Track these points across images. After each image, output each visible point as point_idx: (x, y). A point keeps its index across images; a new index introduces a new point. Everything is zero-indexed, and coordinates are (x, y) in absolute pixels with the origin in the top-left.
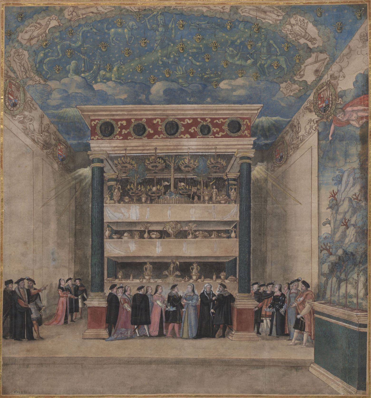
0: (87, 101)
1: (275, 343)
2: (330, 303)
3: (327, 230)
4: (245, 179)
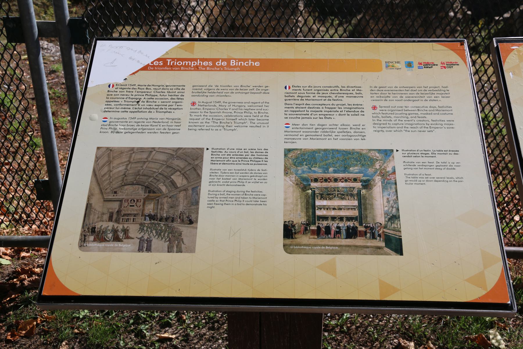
0: (309, 172)
1: (372, 241)
2: (389, 229)
3: (386, 209)
4: (359, 194)
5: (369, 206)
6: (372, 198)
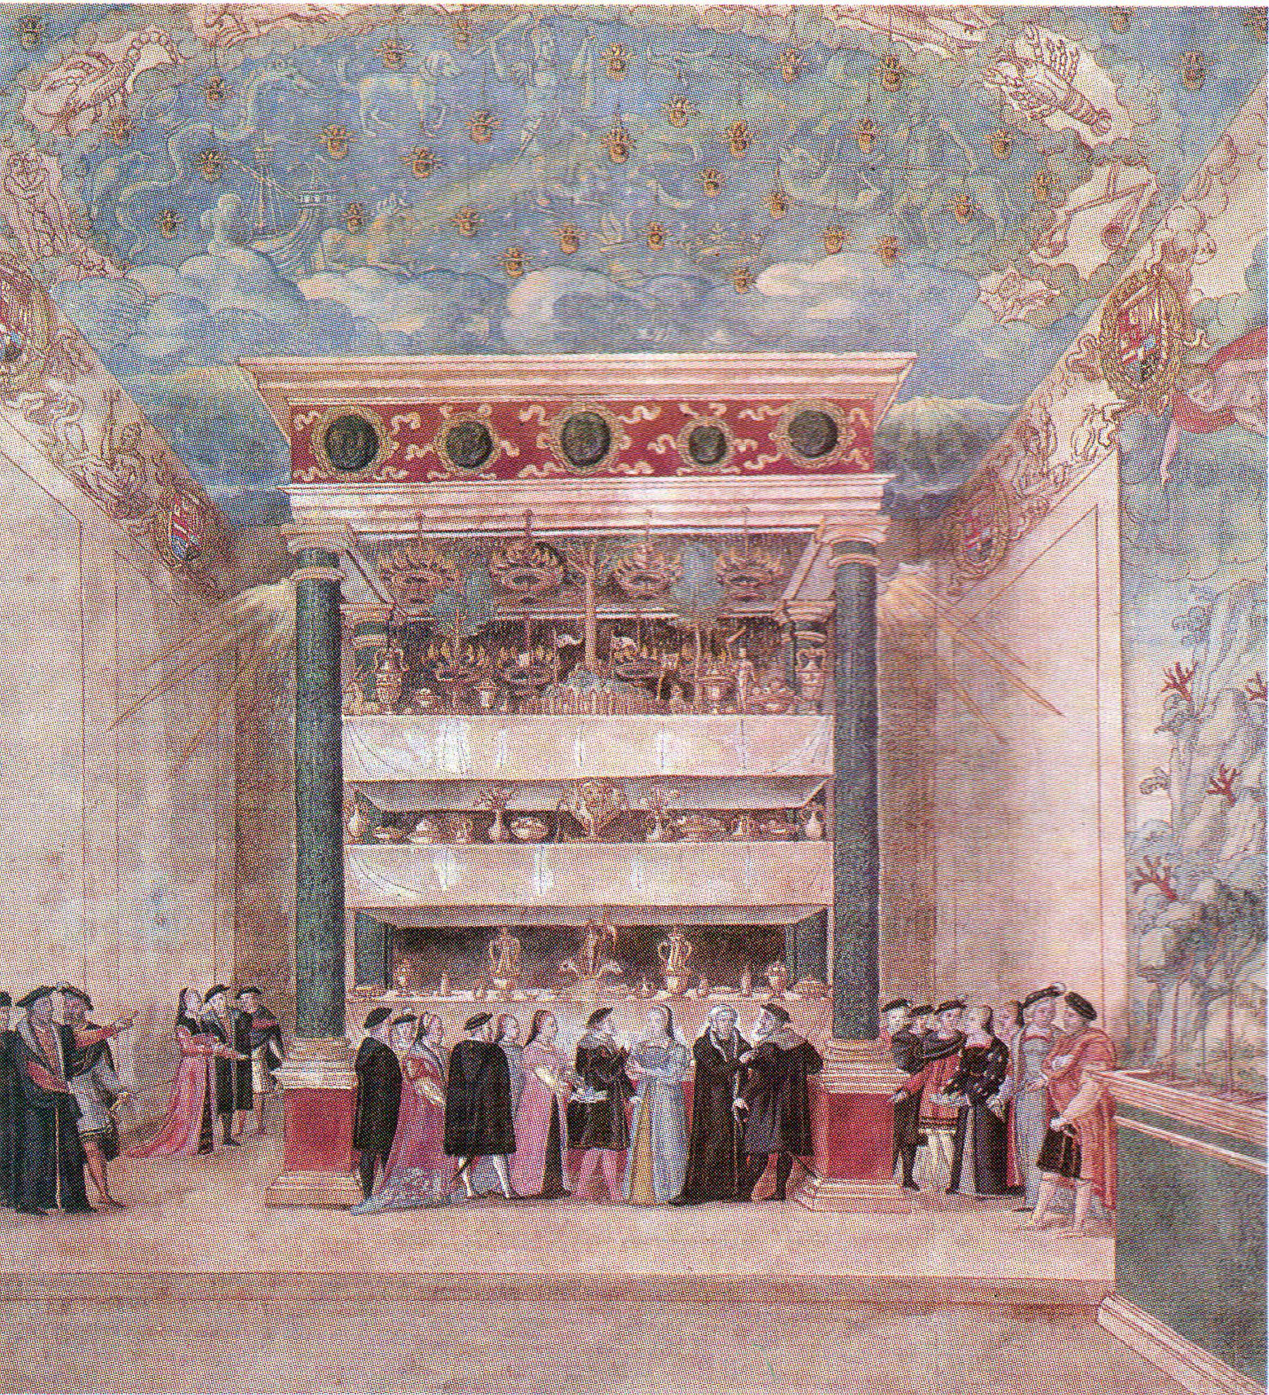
0: (274, 338)
2: (1169, 1074)
3: (1154, 810)
4: (851, 632)
5: (965, 791)
6: (1006, 674)
